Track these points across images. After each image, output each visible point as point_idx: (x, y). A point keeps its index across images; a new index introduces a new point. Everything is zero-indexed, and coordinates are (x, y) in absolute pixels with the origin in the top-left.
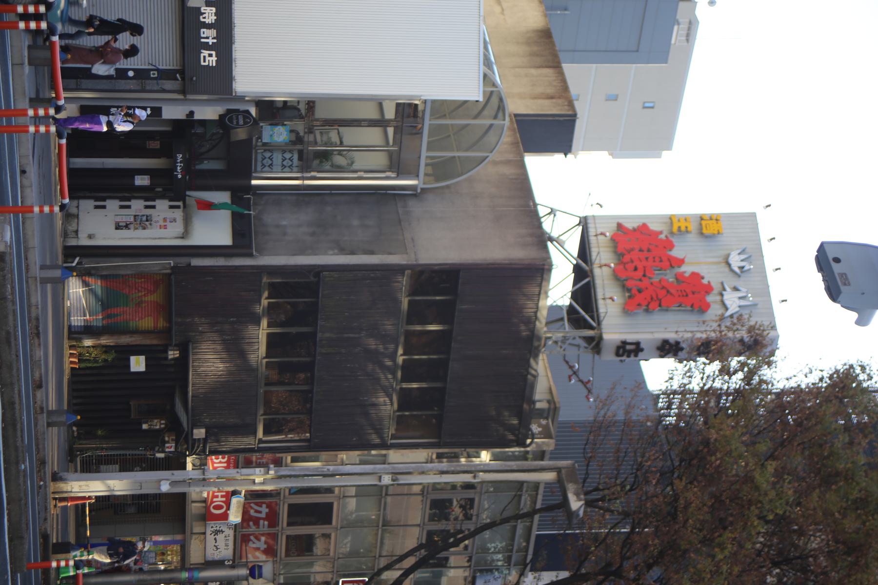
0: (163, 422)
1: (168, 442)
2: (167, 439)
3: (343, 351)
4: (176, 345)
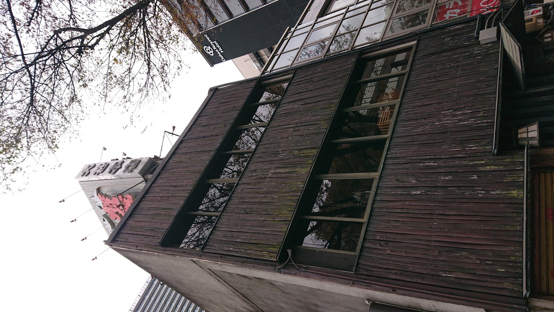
0: (549, 40)
1: (538, 17)
2: (541, 21)
3: (296, 152)
4: (522, 147)
